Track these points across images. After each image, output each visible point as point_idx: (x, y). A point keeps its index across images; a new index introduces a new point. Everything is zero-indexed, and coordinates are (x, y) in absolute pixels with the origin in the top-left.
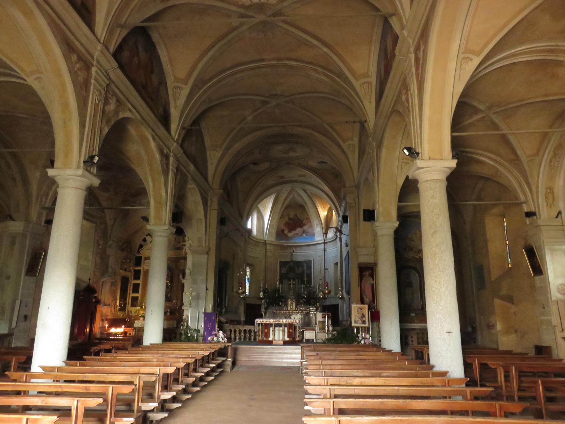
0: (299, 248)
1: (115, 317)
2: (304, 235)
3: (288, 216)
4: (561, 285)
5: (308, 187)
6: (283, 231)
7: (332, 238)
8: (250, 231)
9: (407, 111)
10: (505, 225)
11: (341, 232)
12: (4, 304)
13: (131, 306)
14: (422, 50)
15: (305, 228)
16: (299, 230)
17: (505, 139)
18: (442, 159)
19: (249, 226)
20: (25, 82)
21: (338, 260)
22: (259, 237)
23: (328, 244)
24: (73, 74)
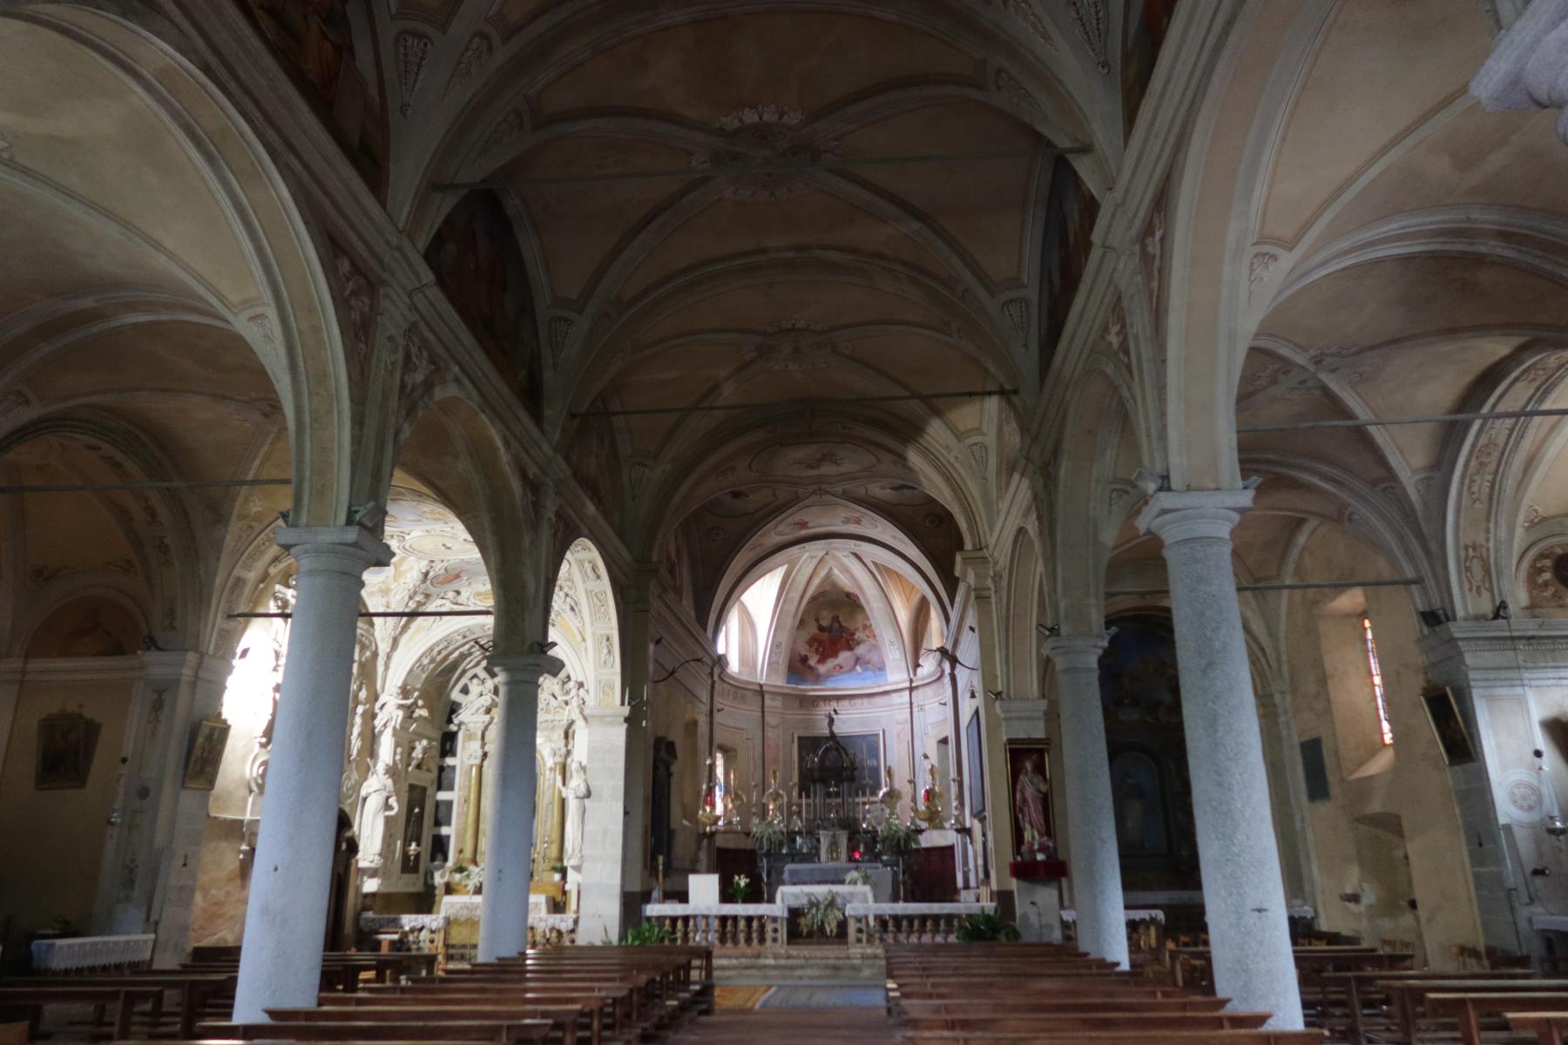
0: (846, 703)
2: (858, 668)
3: (817, 620)
4: (1519, 785)
5: (865, 549)
6: (804, 660)
7: (930, 675)
8: (721, 661)
9: (1124, 371)
10: (1370, 636)
11: (954, 661)
12: (133, 861)
13: (951, 848)
14: (1158, 235)
15: (860, 650)
16: (844, 657)
17: (1361, 436)
19: (721, 649)
20: (226, 326)
21: (949, 731)
22: (744, 678)
23: (920, 691)
24: (342, 304)
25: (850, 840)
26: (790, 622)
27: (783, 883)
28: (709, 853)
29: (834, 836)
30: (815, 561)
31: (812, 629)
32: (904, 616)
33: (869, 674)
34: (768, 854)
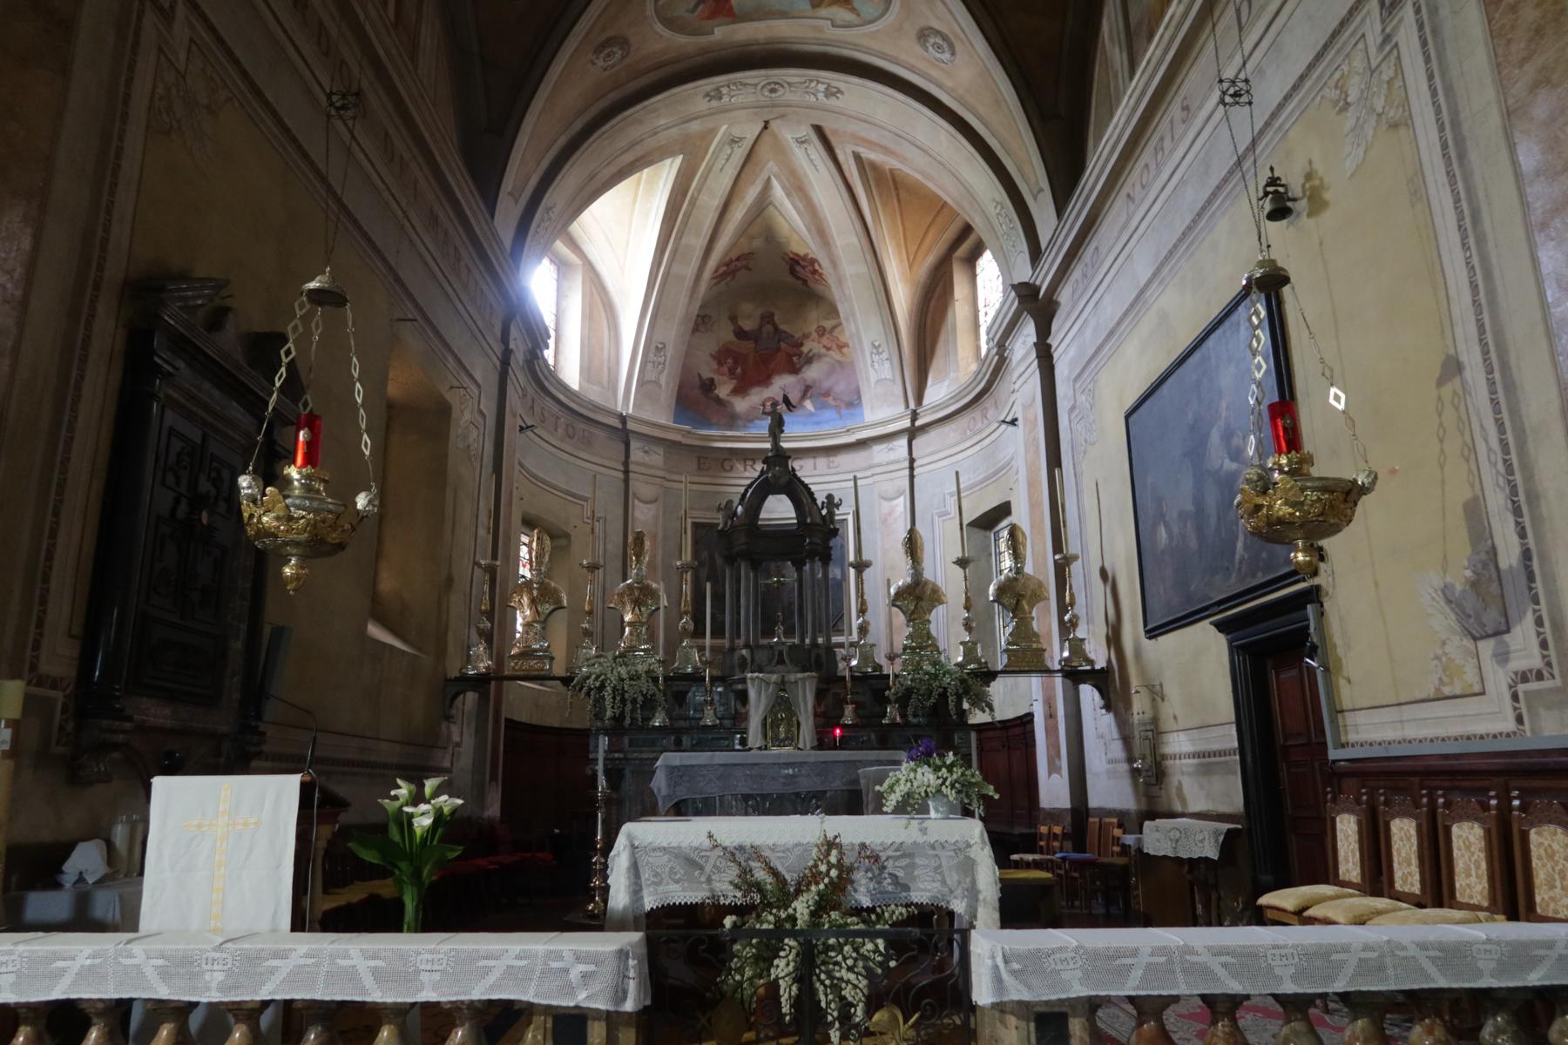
1: (1528, 431)
2: (808, 405)
3: (733, 319)
6: (708, 386)
15: (812, 373)
18: (1498, 65)
25: (820, 695)
26: (683, 306)
27: (647, 809)
28: (480, 731)
29: (782, 685)
30: (739, 153)
31: (725, 334)
32: (903, 297)
33: (829, 414)
34: (616, 729)
